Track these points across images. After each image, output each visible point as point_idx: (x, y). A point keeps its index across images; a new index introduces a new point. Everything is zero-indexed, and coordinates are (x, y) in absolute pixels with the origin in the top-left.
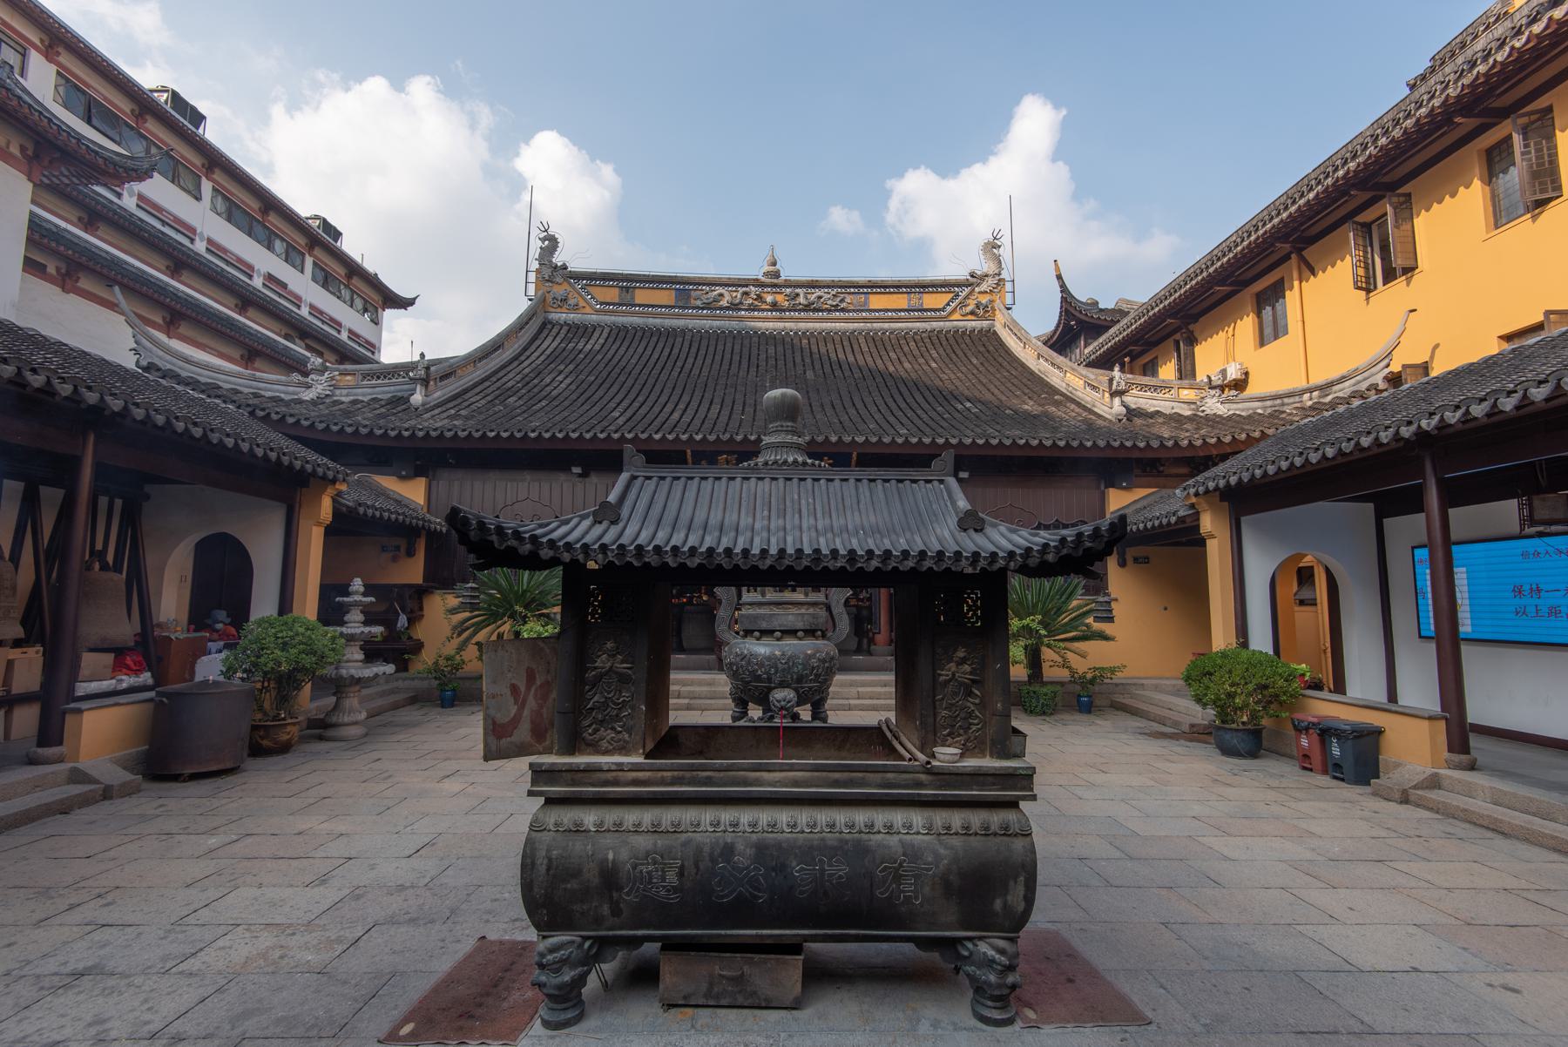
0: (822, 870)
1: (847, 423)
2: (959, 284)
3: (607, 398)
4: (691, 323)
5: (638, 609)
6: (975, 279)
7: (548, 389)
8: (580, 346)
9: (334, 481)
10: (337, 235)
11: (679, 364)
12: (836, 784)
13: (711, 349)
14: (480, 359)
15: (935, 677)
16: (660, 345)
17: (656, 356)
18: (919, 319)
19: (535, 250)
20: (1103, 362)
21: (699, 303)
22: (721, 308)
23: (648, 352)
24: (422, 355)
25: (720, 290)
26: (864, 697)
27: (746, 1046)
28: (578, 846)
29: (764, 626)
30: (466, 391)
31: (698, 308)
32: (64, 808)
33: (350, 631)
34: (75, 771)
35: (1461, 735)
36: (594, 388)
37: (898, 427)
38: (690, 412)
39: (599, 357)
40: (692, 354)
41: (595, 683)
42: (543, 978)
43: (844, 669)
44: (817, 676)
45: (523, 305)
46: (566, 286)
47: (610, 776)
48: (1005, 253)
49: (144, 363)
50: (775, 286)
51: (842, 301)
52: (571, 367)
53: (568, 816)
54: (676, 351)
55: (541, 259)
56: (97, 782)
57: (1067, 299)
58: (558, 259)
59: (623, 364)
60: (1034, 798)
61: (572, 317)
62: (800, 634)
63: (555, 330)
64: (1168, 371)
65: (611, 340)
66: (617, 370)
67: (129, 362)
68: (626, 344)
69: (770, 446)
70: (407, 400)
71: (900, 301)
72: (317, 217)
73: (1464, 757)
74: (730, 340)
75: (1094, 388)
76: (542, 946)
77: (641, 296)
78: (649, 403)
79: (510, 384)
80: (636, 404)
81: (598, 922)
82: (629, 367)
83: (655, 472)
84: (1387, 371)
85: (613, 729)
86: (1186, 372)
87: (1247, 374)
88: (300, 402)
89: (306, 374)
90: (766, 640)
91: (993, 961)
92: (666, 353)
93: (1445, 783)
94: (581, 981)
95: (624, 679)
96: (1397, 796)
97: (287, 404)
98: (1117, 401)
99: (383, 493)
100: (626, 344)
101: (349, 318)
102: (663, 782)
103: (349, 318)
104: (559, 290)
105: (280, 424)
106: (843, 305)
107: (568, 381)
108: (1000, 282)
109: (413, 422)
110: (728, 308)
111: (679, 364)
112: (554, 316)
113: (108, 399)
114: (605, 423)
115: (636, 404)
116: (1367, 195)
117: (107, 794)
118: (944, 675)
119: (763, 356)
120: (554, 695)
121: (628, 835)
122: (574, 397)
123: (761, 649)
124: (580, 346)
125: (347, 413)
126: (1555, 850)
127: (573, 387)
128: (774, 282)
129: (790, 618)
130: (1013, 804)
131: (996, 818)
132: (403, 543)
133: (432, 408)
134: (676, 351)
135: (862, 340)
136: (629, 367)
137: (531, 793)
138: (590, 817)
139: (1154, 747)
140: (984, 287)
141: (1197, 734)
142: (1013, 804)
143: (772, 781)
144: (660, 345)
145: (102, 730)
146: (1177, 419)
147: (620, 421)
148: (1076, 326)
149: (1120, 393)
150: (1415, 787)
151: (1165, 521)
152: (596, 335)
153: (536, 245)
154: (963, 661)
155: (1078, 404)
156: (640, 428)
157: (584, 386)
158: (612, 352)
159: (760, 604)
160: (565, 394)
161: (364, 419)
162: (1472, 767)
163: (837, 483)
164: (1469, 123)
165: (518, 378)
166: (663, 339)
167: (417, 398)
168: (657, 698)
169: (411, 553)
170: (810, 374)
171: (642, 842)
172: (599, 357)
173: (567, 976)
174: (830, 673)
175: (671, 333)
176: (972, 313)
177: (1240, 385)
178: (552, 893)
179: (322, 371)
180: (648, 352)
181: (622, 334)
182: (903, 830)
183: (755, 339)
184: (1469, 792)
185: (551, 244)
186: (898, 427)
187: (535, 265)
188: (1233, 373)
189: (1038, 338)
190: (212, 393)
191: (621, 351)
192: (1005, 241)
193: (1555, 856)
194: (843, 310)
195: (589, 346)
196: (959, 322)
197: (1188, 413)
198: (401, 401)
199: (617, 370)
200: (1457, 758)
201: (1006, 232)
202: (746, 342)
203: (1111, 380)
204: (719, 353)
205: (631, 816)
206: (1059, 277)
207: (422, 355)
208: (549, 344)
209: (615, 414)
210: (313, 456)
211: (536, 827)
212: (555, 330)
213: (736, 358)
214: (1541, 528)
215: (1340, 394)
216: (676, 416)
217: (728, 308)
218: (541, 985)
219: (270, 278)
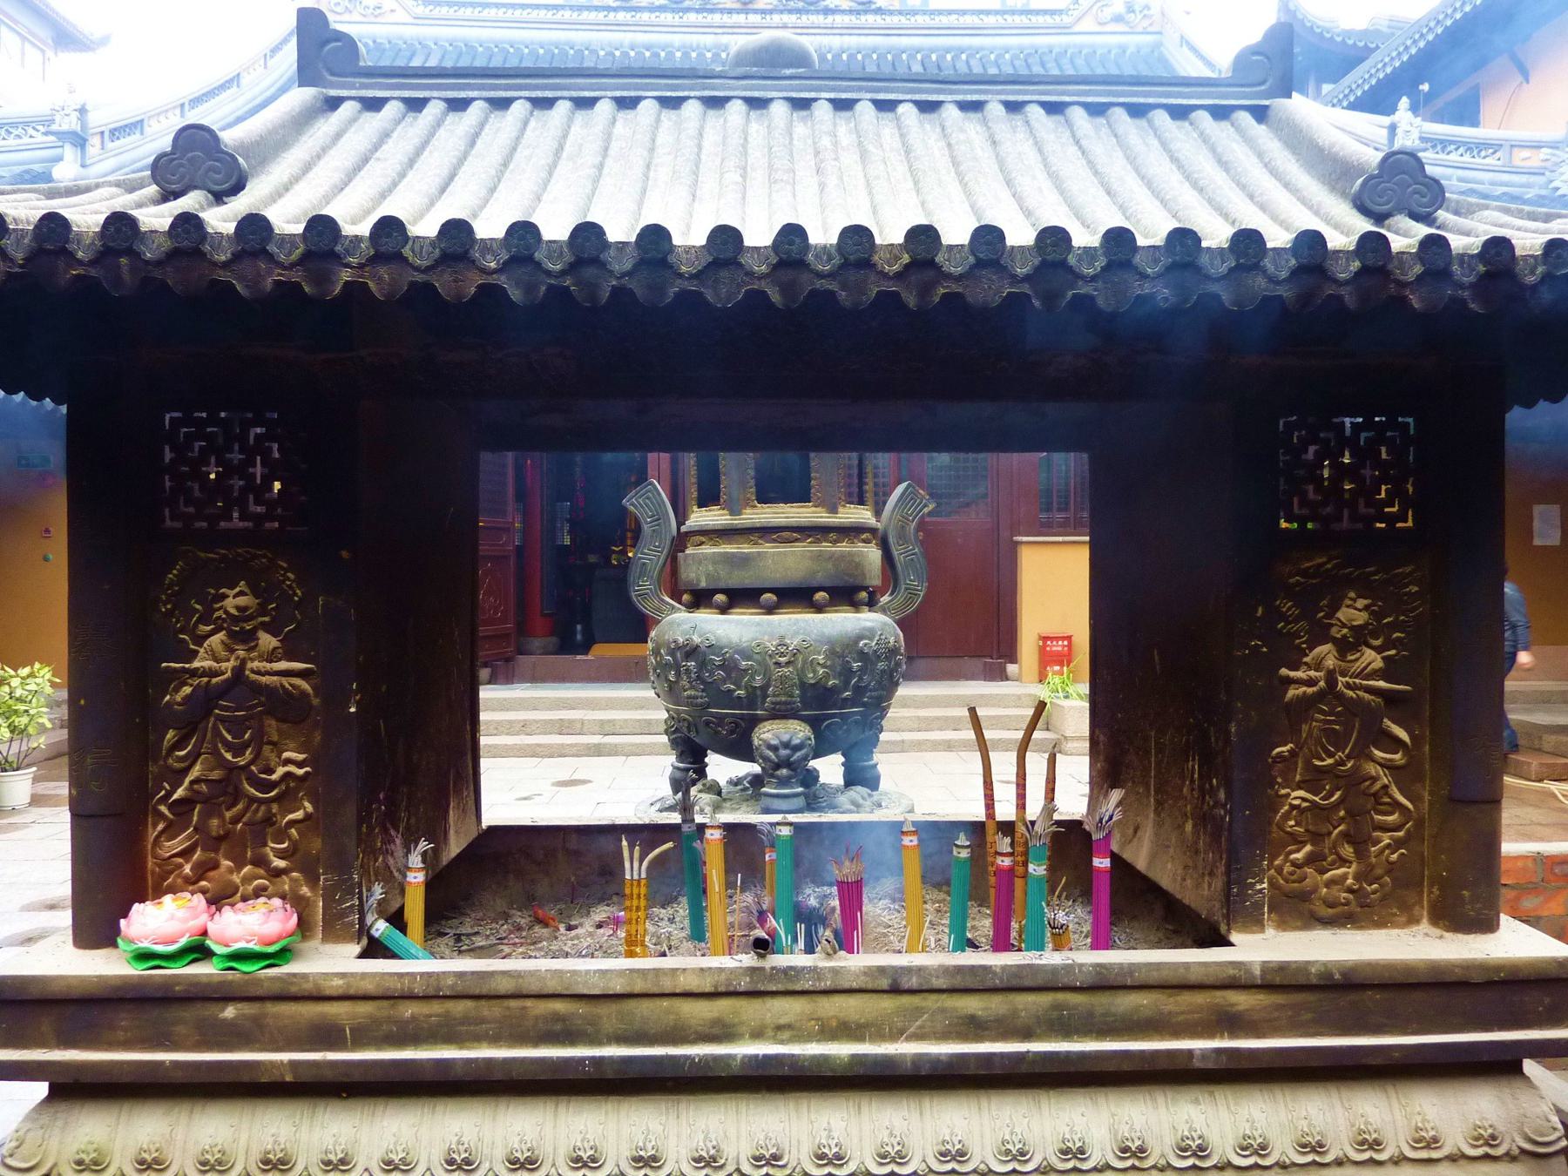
12: (974, 1028)
27: (746, 3)
41: (193, 720)
43: (912, 677)
44: (859, 690)
85: (260, 862)
95: (283, 706)
129: (786, 562)
168: (447, 759)
176: (1118, 19)
203: (1393, 129)
214: (596, 739)
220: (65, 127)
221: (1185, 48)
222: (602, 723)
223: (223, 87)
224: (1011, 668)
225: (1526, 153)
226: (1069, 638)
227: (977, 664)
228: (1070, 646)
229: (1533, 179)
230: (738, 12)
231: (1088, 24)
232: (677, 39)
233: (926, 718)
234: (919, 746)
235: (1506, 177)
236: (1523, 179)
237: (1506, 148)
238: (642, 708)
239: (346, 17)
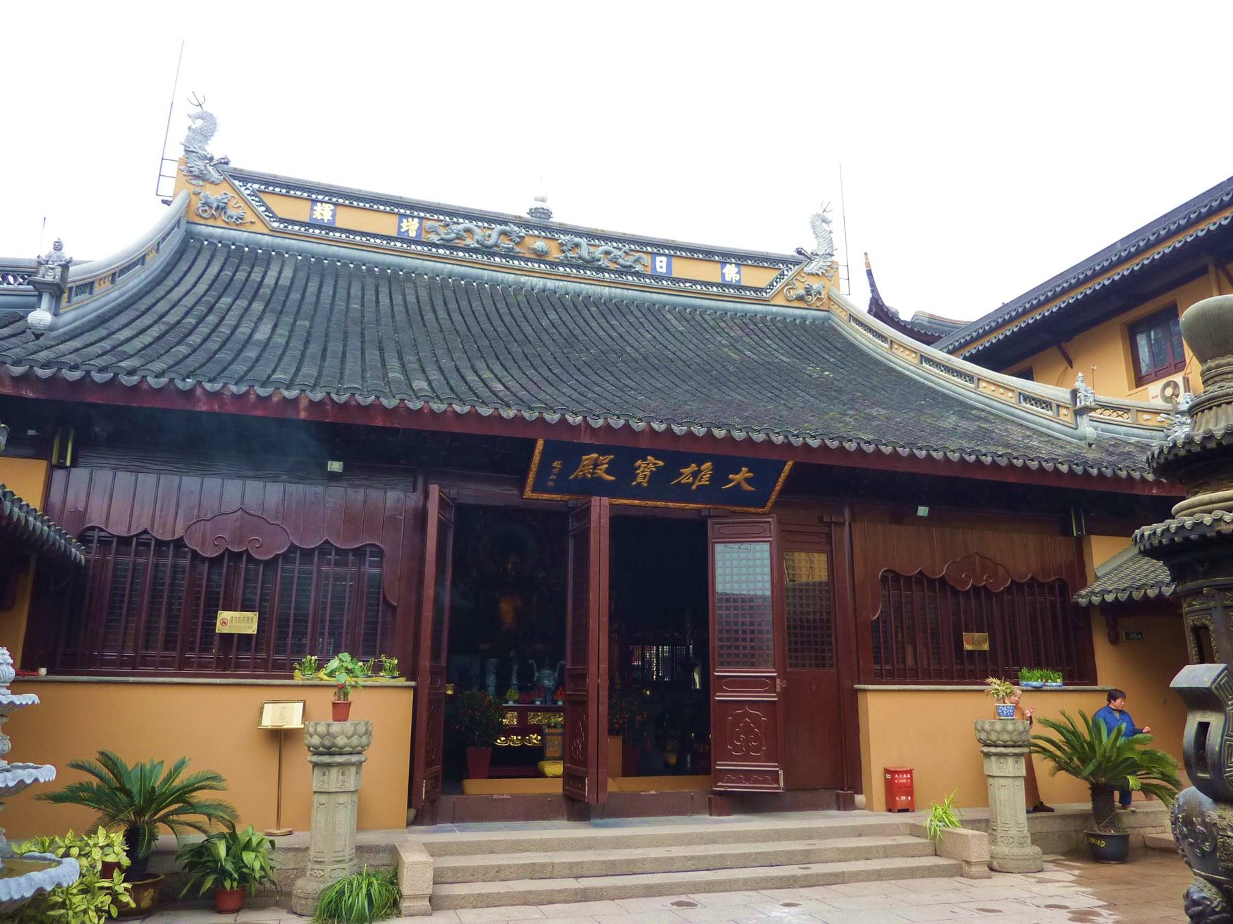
2: (788, 262)
6: (802, 257)
19: (179, 134)
21: (434, 238)
22: (467, 249)
24: (58, 246)
46: (225, 188)
48: (836, 226)
51: (637, 261)
58: (216, 148)
104: (214, 194)
106: (638, 268)
108: (833, 267)
110: (475, 251)
120: (110, 573)
128: (540, 222)
176: (800, 298)
185: (205, 128)
203: (1074, 393)
206: (869, 273)
207: (58, 246)
217: (475, 251)
220: (49, 279)
221: (852, 323)
222: (571, 865)
223: (135, 264)
224: (860, 799)
225: (1147, 416)
226: (910, 772)
227: (829, 796)
228: (911, 778)
229: (1154, 433)
230: (533, 261)
231: (780, 300)
232: (486, 274)
233: (844, 849)
234: (856, 877)
235: (1135, 431)
236: (1148, 433)
237: (1054, 407)
238: (590, 848)
239: (211, 222)
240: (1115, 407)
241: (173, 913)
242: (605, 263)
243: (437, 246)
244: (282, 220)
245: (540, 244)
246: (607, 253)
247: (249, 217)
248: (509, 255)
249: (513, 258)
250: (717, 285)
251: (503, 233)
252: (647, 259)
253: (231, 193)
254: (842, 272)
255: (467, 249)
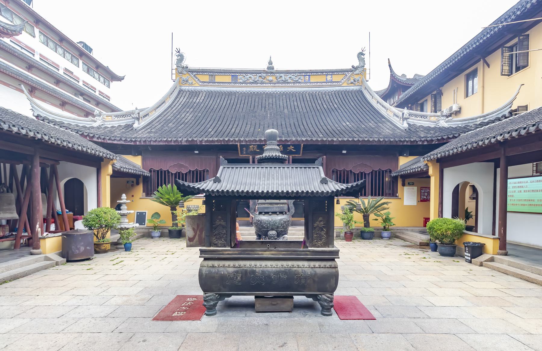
0: (280, 277)
1: (300, 132)
3: (206, 123)
4: (238, 89)
5: (226, 208)
6: (355, 68)
7: (184, 119)
8: (194, 100)
9: (112, 160)
10: (91, 50)
11: (234, 107)
13: (246, 101)
14: (157, 108)
15: (313, 225)
16: (226, 99)
17: (224, 104)
18: (331, 86)
20: (400, 105)
21: (241, 81)
22: (250, 83)
23: (221, 103)
25: (250, 75)
26: (296, 233)
28: (213, 270)
29: (266, 211)
30: (152, 121)
31: (241, 83)
32: (46, 268)
33: (123, 212)
34: (46, 257)
35: (503, 245)
36: (201, 118)
37: (319, 133)
38: (239, 128)
39: (202, 105)
40: (239, 103)
42: (206, 304)
45: (171, 84)
46: (187, 75)
47: (221, 252)
48: (366, 57)
49: (36, 115)
50: (272, 73)
52: (192, 110)
53: (210, 263)
54: (232, 102)
55: (177, 63)
56: (53, 260)
57: (393, 76)
59: (212, 108)
60: (339, 258)
61: (191, 88)
62: (270, 213)
63: (184, 94)
64: (429, 106)
65: (206, 97)
66: (210, 111)
67: (30, 115)
68: (212, 99)
69: (267, 150)
70: (131, 126)
71: (322, 79)
72: (81, 42)
73: (504, 251)
74: (254, 97)
75: (397, 116)
76: (205, 296)
77: (218, 79)
78: (223, 125)
79: (169, 117)
80: (218, 125)
81: (220, 290)
82: (214, 109)
83: (230, 166)
84: (510, 109)
86: (436, 108)
87: (460, 108)
88: (93, 128)
89: (94, 116)
90: (266, 215)
91: (326, 300)
92: (229, 101)
93: (495, 260)
94: (215, 305)
95: (224, 227)
96: (479, 264)
97: (89, 128)
98: (405, 122)
99: (126, 162)
100: (212, 99)
101: (96, 84)
102: (236, 254)
103: (96, 84)
105: (91, 139)
106: (300, 81)
107: (191, 116)
109: (135, 135)
110: (253, 83)
111: (234, 107)
112: (183, 88)
113: (43, 136)
114: (206, 134)
115: (218, 125)
116: (511, 36)
117: (57, 264)
118: (315, 225)
119: (267, 103)
121: (228, 267)
122: (194, 123)
123: (264, 218)
124: (194, 100)
125: (111, 132)
126: (521, 279)
127: (193, 118)
129: (275, 208)
130: (333, 260)
131: (328, 264)
132: (135, 180)
133: (141, 129)
134: (232, 102)
135: (307, 95)
136: (214, 109)
137: (200, 257)
138: (216, 263)
139: (407, 250)
140: (357, 72)
141: (423, 246)
142: (333, 260)
143: (267, 254)
144: (226, 99)
145: (51, 243)
146: (428, 129)
147: (212, 133)
148: (397, 85)
149: (407, 119)
150: (485, 261)
151: (417, 170)
152: (200, 95)
153: (175, 58)
154: (321, 221)
155: (391, 123)
156: (220, 135)
157: (197, 118)
158: (207, 103)
159: (264, 204)
160: (191, 121)
161: (117, 134)
162: (506, 254)
163: (286, 168)
164: (503, 43)
165: (172, 115)
166: (227, 97)
167: (136, 125)
169: (138, 184)
170: (286, 111)
171: (231, 270)
172: (202, 105)
173: (212, 303)
174: (288, 225)
175: (230, 94)
177: (458, 112)
178: (206, 281)
179: (100, 115)
180: (221, 103)
181: (211, 95)
182: (304, 267)
183: (264, 96)
184: (502, 262)
185: (181, 58)
186: (319, 133)
187: (175, 67)
188: (455, 108)
189: (377, 93)
190: (61, 125)
191: (211, 102)
192: (366, 53)
193: (520, 280)
194: (299, 83)
195: (198, 101)
196: (346, 87)
197: (433, 126)
198: (129, 127)
199: (210, 111)
200: (501, 251)
201: (367, 49)
202: (260, 97)
204: (250, 102)
205: (227, 263)
206: (390, 66)
208: (183, 100)
209: (210, 130)
210: (105, 151)
211: (202, 266)
212: (184, 94)
213: (256, 104)
215: (491, 119)
216: (233, 130)
218: (205, 305)
219: (66, 69)
240: (489, 99)
241: (235, 311)
242: (289, 81)
243: (243, 83)
244: (202, 82)
245: (270, 78)
246: (290, 77)
247: (194, 82)
248: (262, 83)
249: (263, 83)
250: (325, 82)
251: (260, 76)
252: (302, 77)
253: (189, 76)
254: (368, 72)
255: (250, 83)
